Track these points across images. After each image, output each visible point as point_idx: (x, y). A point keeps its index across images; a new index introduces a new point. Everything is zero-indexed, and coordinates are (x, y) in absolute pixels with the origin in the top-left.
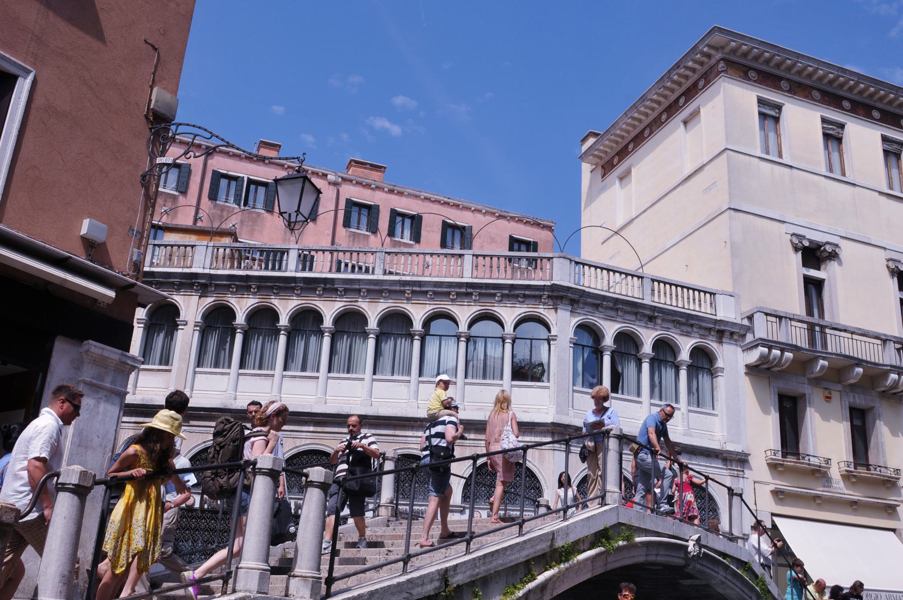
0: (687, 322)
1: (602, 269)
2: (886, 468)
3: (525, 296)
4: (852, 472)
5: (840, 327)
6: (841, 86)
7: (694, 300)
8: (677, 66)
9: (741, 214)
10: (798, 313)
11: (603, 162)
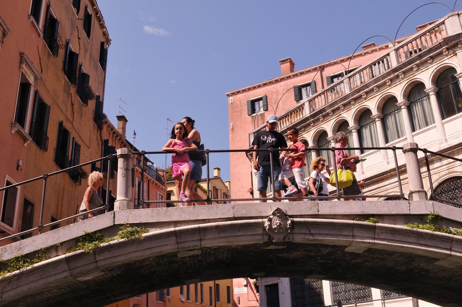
3: (432, 58)
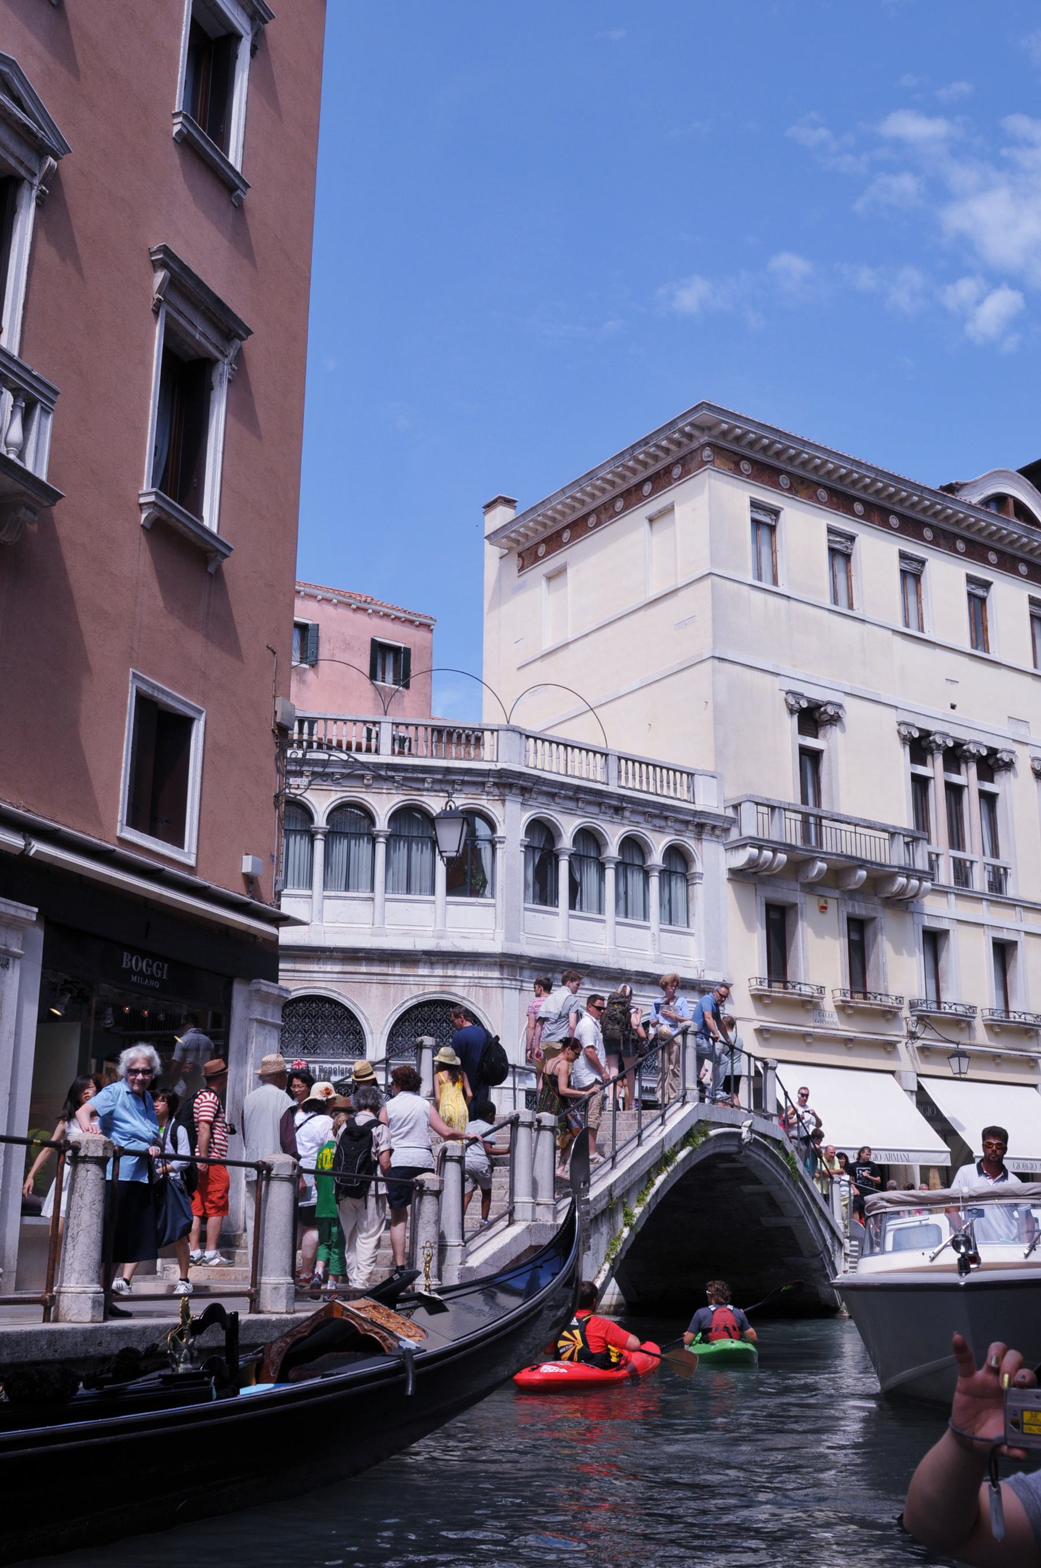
0: (660, 814)
1: (558, 744)
2: (887, 995)
3: (464, 783)
4: (848, 1002)
5: (842, 818)
6: (854, 483)
7: (668, 783)
8: (645, 441)
9: (727, 665)
10: (792, 802)
11: (520, 549)
